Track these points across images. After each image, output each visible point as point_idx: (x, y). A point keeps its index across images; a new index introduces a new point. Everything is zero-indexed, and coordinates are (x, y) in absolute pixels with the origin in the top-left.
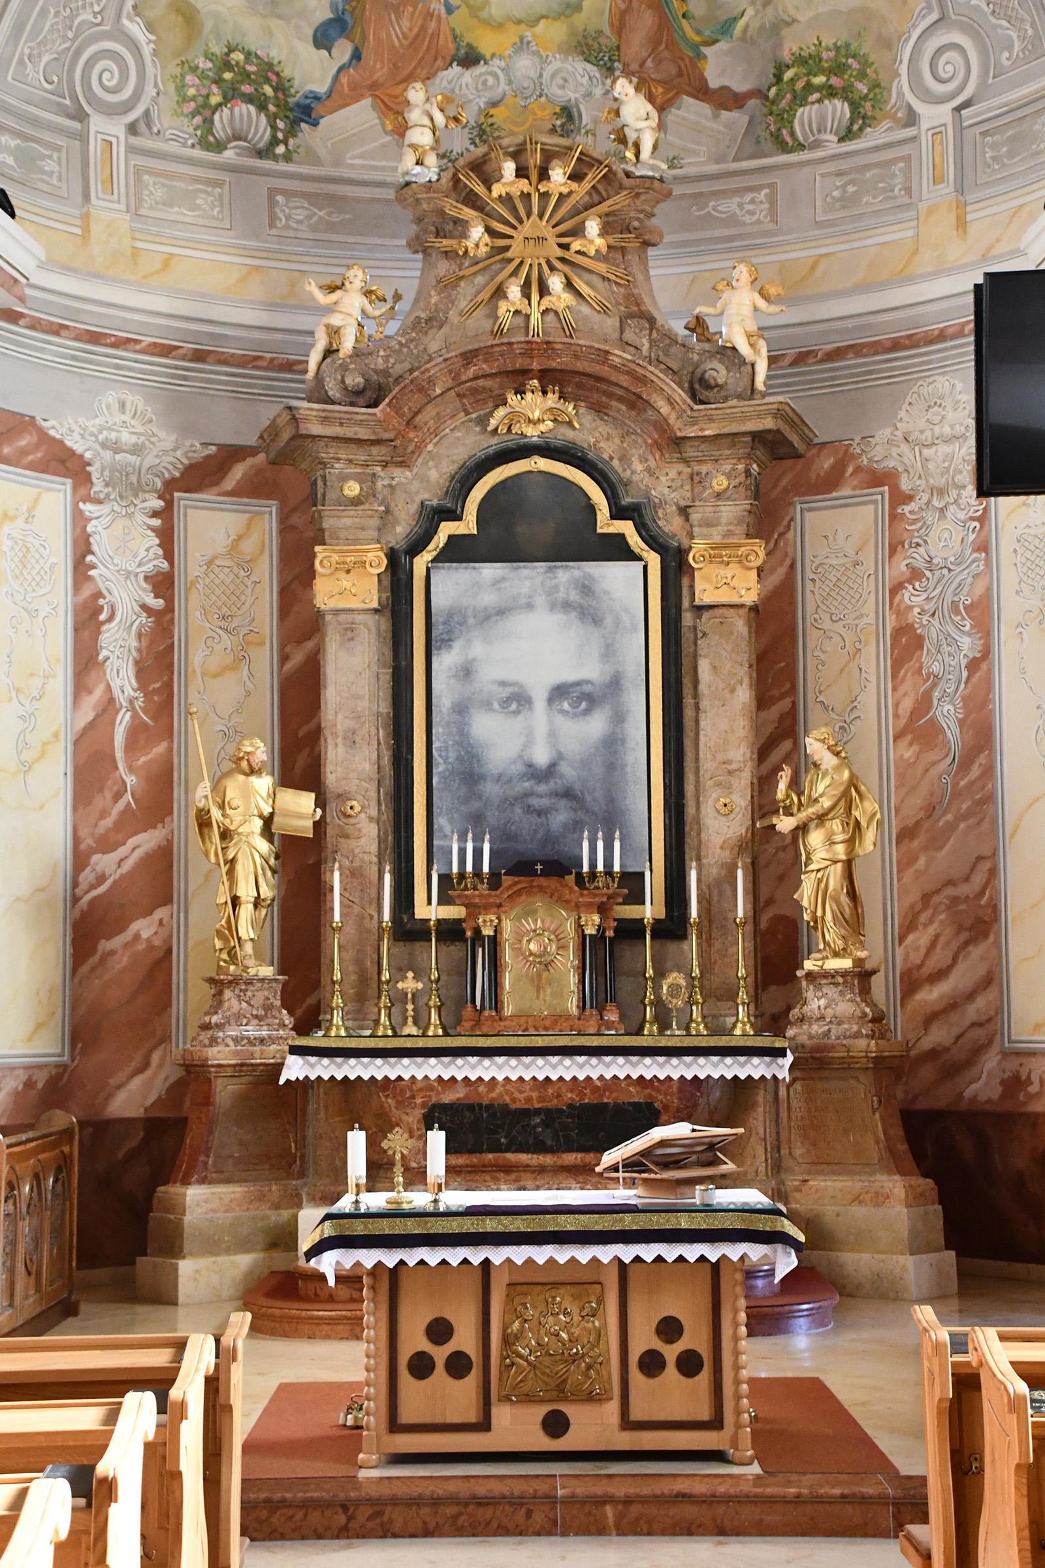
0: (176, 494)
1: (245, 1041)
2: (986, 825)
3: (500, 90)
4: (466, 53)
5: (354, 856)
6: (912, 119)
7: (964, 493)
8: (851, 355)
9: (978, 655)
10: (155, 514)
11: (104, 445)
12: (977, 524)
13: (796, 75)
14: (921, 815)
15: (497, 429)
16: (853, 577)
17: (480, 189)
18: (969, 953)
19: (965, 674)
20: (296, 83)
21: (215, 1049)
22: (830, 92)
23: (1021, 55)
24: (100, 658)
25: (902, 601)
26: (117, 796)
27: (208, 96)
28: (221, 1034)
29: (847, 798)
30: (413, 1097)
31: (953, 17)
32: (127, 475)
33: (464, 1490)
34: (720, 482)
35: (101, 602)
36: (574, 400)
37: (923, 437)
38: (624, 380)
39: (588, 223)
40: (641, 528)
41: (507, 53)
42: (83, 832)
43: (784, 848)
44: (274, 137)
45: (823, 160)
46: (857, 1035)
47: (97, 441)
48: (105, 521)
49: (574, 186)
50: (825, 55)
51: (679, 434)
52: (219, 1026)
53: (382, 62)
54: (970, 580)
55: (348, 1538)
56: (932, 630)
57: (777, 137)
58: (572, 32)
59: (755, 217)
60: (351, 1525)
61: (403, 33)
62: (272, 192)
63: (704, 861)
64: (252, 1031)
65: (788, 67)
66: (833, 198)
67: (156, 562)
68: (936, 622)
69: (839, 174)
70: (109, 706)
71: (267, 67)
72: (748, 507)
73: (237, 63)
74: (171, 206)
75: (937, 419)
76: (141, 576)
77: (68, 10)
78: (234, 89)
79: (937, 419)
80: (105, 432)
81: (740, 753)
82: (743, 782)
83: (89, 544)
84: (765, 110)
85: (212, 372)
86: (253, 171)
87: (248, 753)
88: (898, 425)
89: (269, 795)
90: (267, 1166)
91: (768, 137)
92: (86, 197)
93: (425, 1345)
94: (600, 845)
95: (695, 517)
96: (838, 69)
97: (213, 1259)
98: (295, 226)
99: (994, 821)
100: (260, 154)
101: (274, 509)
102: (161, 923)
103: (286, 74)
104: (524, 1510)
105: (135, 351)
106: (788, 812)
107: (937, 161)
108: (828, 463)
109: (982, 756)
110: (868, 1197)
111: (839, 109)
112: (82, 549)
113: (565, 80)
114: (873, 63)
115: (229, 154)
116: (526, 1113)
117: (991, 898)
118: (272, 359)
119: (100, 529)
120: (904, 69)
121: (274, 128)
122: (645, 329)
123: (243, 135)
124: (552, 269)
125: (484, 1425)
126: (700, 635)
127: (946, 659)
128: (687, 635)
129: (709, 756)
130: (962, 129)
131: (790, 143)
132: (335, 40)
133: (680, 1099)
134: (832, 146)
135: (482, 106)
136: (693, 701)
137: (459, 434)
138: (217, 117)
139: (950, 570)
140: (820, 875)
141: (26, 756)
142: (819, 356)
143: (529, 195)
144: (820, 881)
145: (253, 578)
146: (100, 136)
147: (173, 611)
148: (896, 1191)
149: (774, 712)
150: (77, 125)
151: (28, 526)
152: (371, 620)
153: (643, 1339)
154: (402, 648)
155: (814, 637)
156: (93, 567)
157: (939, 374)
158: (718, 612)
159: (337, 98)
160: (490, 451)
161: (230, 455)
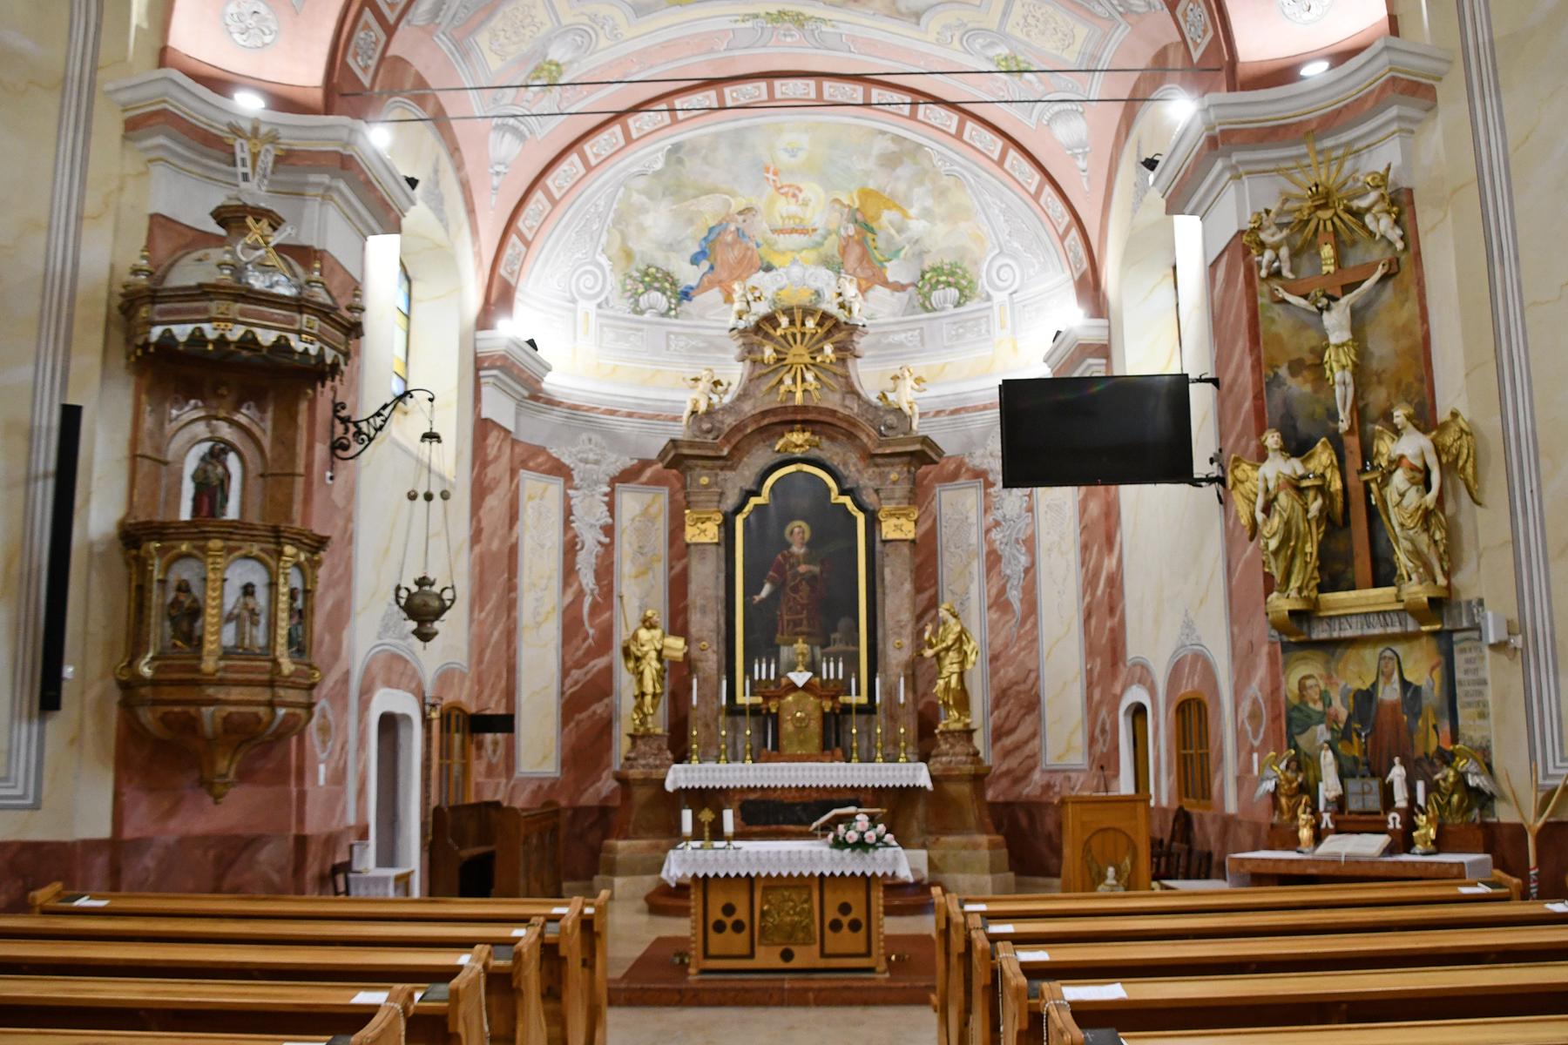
6: (989, 298)
11: (581, 460)
17: (771, 331)
22: (949, 284)
26: (585, 640)
29: (959, 640)
33: (739, 985)
34: (893, 476)
38: (844, 425)
40: (855, 500)
56: (1006, 552)
64: (651, 761)
81: (906, 616)
93: (720, 916)
96: (953, 274)
106: (931, 646)
108: (952, 467)
111: (953, 293)
112: (568, 512)
115: (647, 316)
116: (793, 805)
125: (751, 956)
134: (951, 309)
141: (539, 619)
149: (926, 595)
152: (714, 548)
153: (831, 914)
155: (946, 556)
159: (702, 287)
161: (645, 464)
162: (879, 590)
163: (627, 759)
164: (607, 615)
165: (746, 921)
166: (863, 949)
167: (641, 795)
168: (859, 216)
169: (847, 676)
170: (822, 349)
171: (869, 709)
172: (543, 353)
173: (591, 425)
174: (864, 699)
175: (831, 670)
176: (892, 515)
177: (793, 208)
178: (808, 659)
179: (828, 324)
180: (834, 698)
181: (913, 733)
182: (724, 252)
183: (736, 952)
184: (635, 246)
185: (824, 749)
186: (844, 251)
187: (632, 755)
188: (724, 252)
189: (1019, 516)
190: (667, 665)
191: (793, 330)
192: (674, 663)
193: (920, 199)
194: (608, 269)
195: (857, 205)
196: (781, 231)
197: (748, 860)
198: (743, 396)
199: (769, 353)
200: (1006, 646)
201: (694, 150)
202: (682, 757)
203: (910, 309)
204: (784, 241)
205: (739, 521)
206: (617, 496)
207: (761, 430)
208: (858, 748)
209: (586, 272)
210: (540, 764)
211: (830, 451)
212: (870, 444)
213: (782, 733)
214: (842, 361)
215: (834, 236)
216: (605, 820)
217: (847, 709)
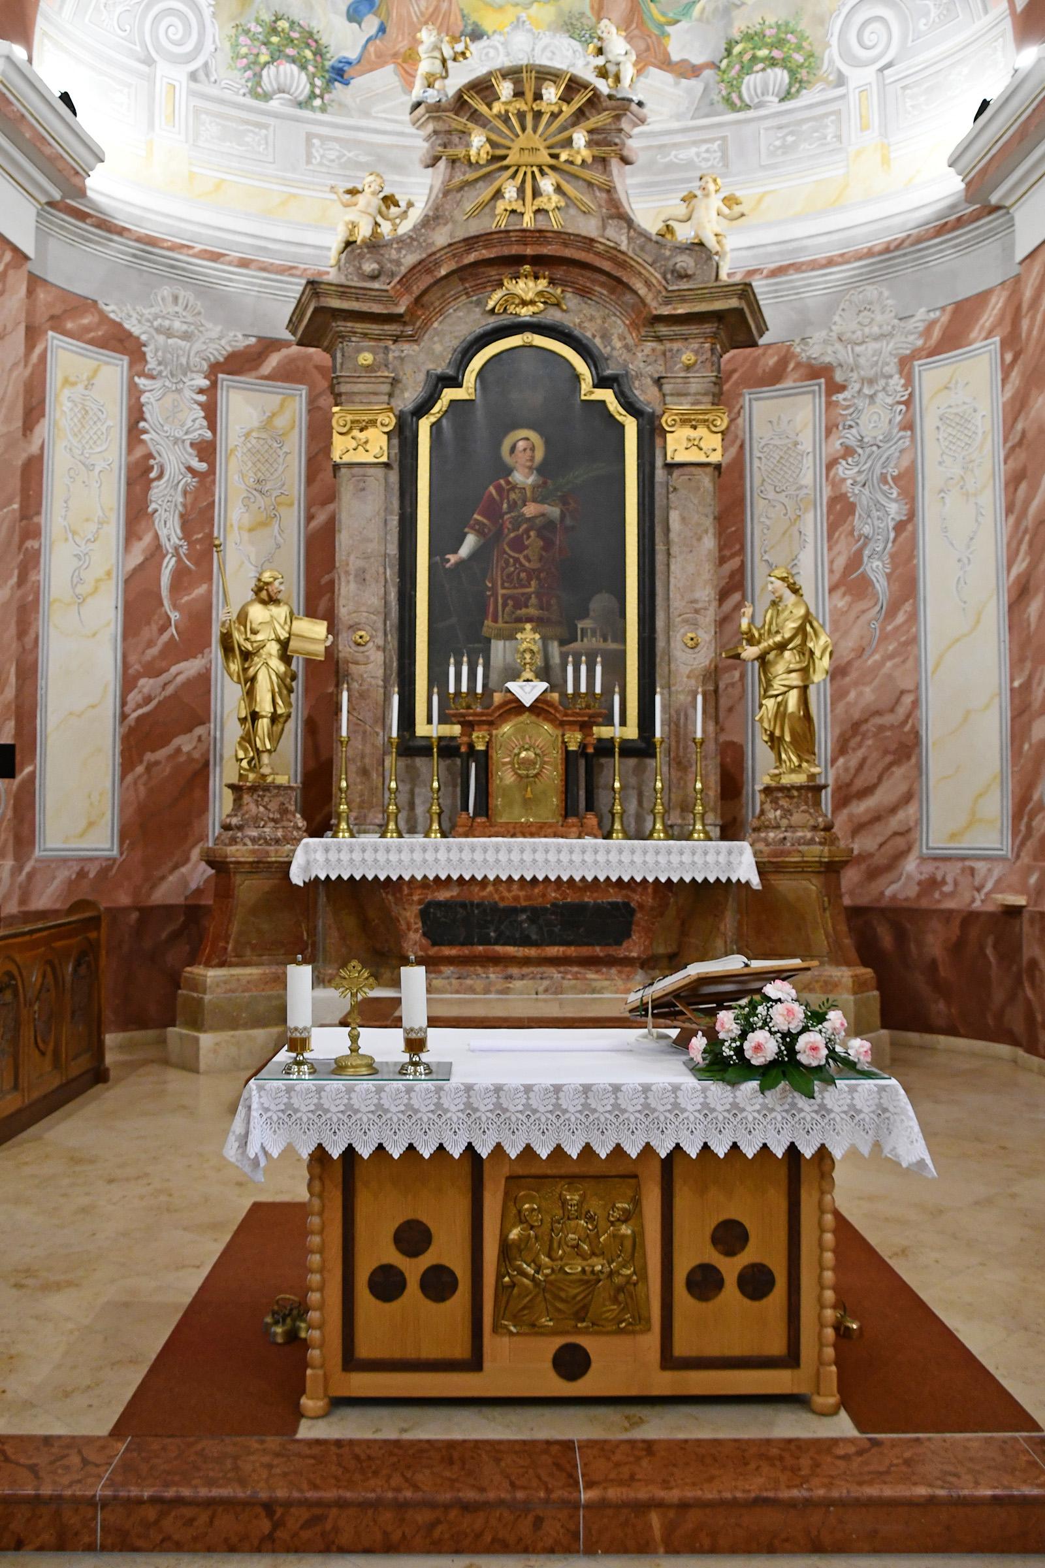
0: (220, 376)
1: (261, 842)
2: (910, 664)
5: (363, 680)
6: (841, 81)
7: (892, 382)
8: (791, 272)
9: (904, 518)
10: (201, 391)
11: (158, 330)
12: (903, 407)
13: (744, 49)
14: (852, 655)
15: (494, 308)
16: (794, 455)
17: (483, 108)
18: (893, 773)
19: (892, 535)
20: (332, 49)
21: (234, 848)
22: (773, 62)
23: (937, 20)
24: (150, 510)
25: (836, 474)
26: (163, 629)
27: (258, 55)
28: (239, 834)
29: (801, 630)
30: (411, 895)
32: (178, 357)
34: (687, 357)
35: (152, 462)
36: (561, 285)
38: (606, 266)
39: (575, 136)
41: (506, 30)
42: (132, 658)
43: (733, 685)
44: (313, 92)
46: (811, 842)
47: (152, 326)
48: (158, 394)
49: (565, 107)
50: (768, 32)
51: (655, 312)
52: (240, 828)
53: (403, 35)
54: (897, 454)
55: (274, 1551)
56: (862, 498)
57: (728, 100)
58: (560, 13)
60: (278, 1534)
62: (309, 137)
63: (673, 689)
65: (737, 42)
67: (200, 432)
68: (866, 491)
69: (780, 128)
70: (156, 552)
72: (714, 379)
73: (283, 30)
76: (188, 443)
78: (280, 51)
80: (159, 320)
81: (705, 594)
82: (707, 620)
83: (143, 412)
84: (718, 79)
85: (253, 277)
86: (297, 119)
87: (267, 584)
88: (834, 327)
89: (285, 622)
90: (282, 951)
92: (151, 125)
93: (394, 1257)
94: (583, 668)
95: (667, 388)
97: (232, 1033)
99: (917, 660)
100: (300, 105)
101: (304, 393)
102: (200, 739)
103: (323, 42)
104: (530, 1518)
105: (189, 255)
106: (752, 641)
108: (772, 361)
109: (907, 604)
110: (817, 986)
111: (780, 76)
112: (136, 415)
113: (553, 53)
115: (274, 104)
116: (514, 911)
117: (913, 726)
118: (305, 270)
119: (152, 400)
120: (834, 41)
121: (313, 85)
125: (475, 1363)
126: (671, 489)
127: (876, 523)
128: (659, 491)
129: (678, 596)
130: (885, 85)
132: (365, 15)
133: (654, 899)
134: (774, 105)
136: (664, 548)
137: (461, 314)
138: (265, 73)
139: (879, 447)
140: (780, 699)
141: (80, 589)
142: (765, 272)
143: (525, 112)
144: (779, 704)
145: (285, 449)
146: (165, 80)
147: (214, 474)
148: (844, 980)
150: (144, 68)
151: (86, 392)
152: (380, 472)
154: (408, 497)
155: (760, 505)
156: (145, 432)
158: (687, 470)
159: (367, 62)
160: (489, 327)
162: (660, 547)
163: (226, 827)
164: (201, 590)
165: (461, 1270)
166: (777, 1346)
167: (248, 889)
169: (608, 691)
170: (569, 142)
171: (642, 748)
172: (85, 119)
173: (179, 274)
174: (631, 732)
175: (581, 679)
176: (684, 422)
178: (539, 662)
179: (580, 100)
180: (585, 727)
181: (713, 793)
183: (429, 1352)
185: (566, 816)
187: (235, 821)
189: (887, 439)
190: (297, 665)
191: (521, 105)
192: (310, 663)
197: (470, 1109)
198: (431, 220)
199: (478, 140)
200: (861, 651)
202: (320, 826)
203: (705, 106)
205: (424, 426)
206: (221, 395)
207: (462, 273)
208: (624, 812)
210: (82, 835)
211: (576, 313)
212: (649, 298)
213: (495, 784)
214: (602, 161)
216: (194, 929)
217: (605, 748)
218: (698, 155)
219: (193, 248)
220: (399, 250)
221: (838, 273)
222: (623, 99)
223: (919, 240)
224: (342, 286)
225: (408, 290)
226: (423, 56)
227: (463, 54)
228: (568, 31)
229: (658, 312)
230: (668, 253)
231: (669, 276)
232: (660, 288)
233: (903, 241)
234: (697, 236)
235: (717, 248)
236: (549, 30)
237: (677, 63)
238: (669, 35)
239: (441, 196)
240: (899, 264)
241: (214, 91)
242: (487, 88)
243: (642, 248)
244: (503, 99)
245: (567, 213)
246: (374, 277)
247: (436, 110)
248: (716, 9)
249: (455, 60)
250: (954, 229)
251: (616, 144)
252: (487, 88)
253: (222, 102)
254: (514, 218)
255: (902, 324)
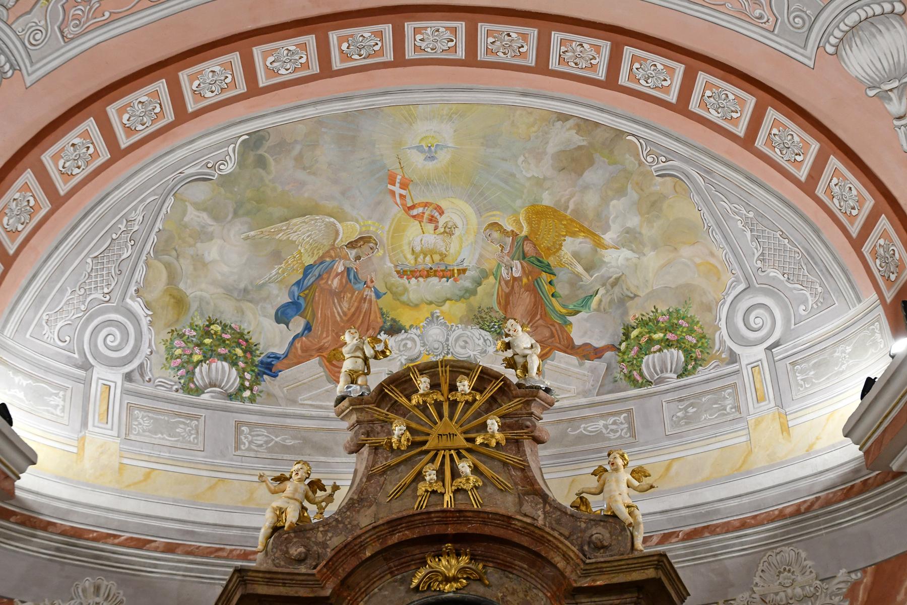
3: (417, 350)
4: (391, 325)
6: (733, 358)
8: (707, 534)
13: (640, 333)
15: (418, 586)
17: (403, 400)
20: (261, 347)
22: (668, 344)
23: (815, 306)
27: (192, 354)
31: (758, 286)
36: (482, 560)
37: (778, 598)
38: (525, 541)
39: (489, 422)
41: (421, 324)
44: (242, 385)
45: (667, 391)
50: (661, 319)
51: (575, 585)
53: (327, 332)
57: (629, 377)
58: (470, 309)
59: (618, 434)
61: (343, 312)
62: (238, 424)
66: (678, 417)
69: (680, 400)
71: (238, 336)
73: (216, 333)
74: (156, 433)
75: (788, 582)
77: (82, 291)
78: (212, 351)
79: (788, 582)
84: (619, 359)
88: (755, 589)
91: (623, 377)
92: (84, 424)
98: (256, 448)
100: (230, 397)
103: (253, 341)
107: (758, 386)
111: (676, 356)
113: (466, 342)
114: (698, 322)
115: (205, 397)
118: (232, 551)
121: (243, 378)
122: (540, 503)
123: (218, 383)
124: (461, 457)
131: (640, 381)
132: (292, 317)
134: (673, 381)
135: (404, 362)
137: (386, 593)
138: (197, 370)
146: (101, 381)
157: (784, 545)
159: (292, 357)
168: (528, 248)
170: (483, 427)
177: (431, 238)
179: (492, 389)
182: (327, 299)
184: (190, 289)
186: (506, 302)
188: (327, 299)
193: (621, 215)
194: (144, 322)
195: (525, 232)
196: (414, 274)
198: (354, 504)
201: (282, 147)
203: (609, 383)
204: (416, 288)
207: (386, 553)
209: (110, 323)
212: (568, 571)
214: (516, 443)
215: (492, 279)
218: (606, 426)
219: (120, 536)
220: (325, 533)
221: (753, 535)
222: (531, 387)
223: (828, 503)
224: (269, 572)
225: (334, 572)
226: (347, 356)
227: (383, 352)
228: (479, 323)
229: (579, 585)
230: (583, 525)
231: (586, 548)
232: (578, 561)
233: (813, 503)
234: (610, 508)
235: (631, 520)
236: (461, 322)
237: (580, 347)
238: (571, 324)
239: (364, 480)
240: (811, 526)
241: (148, 389)
242: (406, 382)
243: (558, 522)
244: (421, 392)
245: (485, 491)
246: (300, 560)
247: (359, 403)
248: (611, 302)
249: (376, 358)
250: (861, 492)
251: (528, 427)
252: (406, 382)
253: (155, 398)
254: (434, 498)
255: (825, 586)
